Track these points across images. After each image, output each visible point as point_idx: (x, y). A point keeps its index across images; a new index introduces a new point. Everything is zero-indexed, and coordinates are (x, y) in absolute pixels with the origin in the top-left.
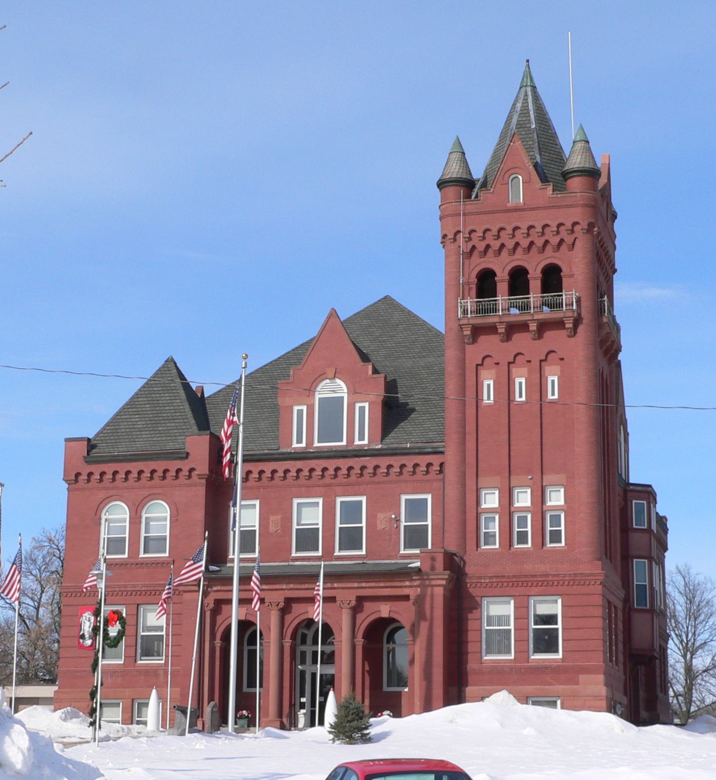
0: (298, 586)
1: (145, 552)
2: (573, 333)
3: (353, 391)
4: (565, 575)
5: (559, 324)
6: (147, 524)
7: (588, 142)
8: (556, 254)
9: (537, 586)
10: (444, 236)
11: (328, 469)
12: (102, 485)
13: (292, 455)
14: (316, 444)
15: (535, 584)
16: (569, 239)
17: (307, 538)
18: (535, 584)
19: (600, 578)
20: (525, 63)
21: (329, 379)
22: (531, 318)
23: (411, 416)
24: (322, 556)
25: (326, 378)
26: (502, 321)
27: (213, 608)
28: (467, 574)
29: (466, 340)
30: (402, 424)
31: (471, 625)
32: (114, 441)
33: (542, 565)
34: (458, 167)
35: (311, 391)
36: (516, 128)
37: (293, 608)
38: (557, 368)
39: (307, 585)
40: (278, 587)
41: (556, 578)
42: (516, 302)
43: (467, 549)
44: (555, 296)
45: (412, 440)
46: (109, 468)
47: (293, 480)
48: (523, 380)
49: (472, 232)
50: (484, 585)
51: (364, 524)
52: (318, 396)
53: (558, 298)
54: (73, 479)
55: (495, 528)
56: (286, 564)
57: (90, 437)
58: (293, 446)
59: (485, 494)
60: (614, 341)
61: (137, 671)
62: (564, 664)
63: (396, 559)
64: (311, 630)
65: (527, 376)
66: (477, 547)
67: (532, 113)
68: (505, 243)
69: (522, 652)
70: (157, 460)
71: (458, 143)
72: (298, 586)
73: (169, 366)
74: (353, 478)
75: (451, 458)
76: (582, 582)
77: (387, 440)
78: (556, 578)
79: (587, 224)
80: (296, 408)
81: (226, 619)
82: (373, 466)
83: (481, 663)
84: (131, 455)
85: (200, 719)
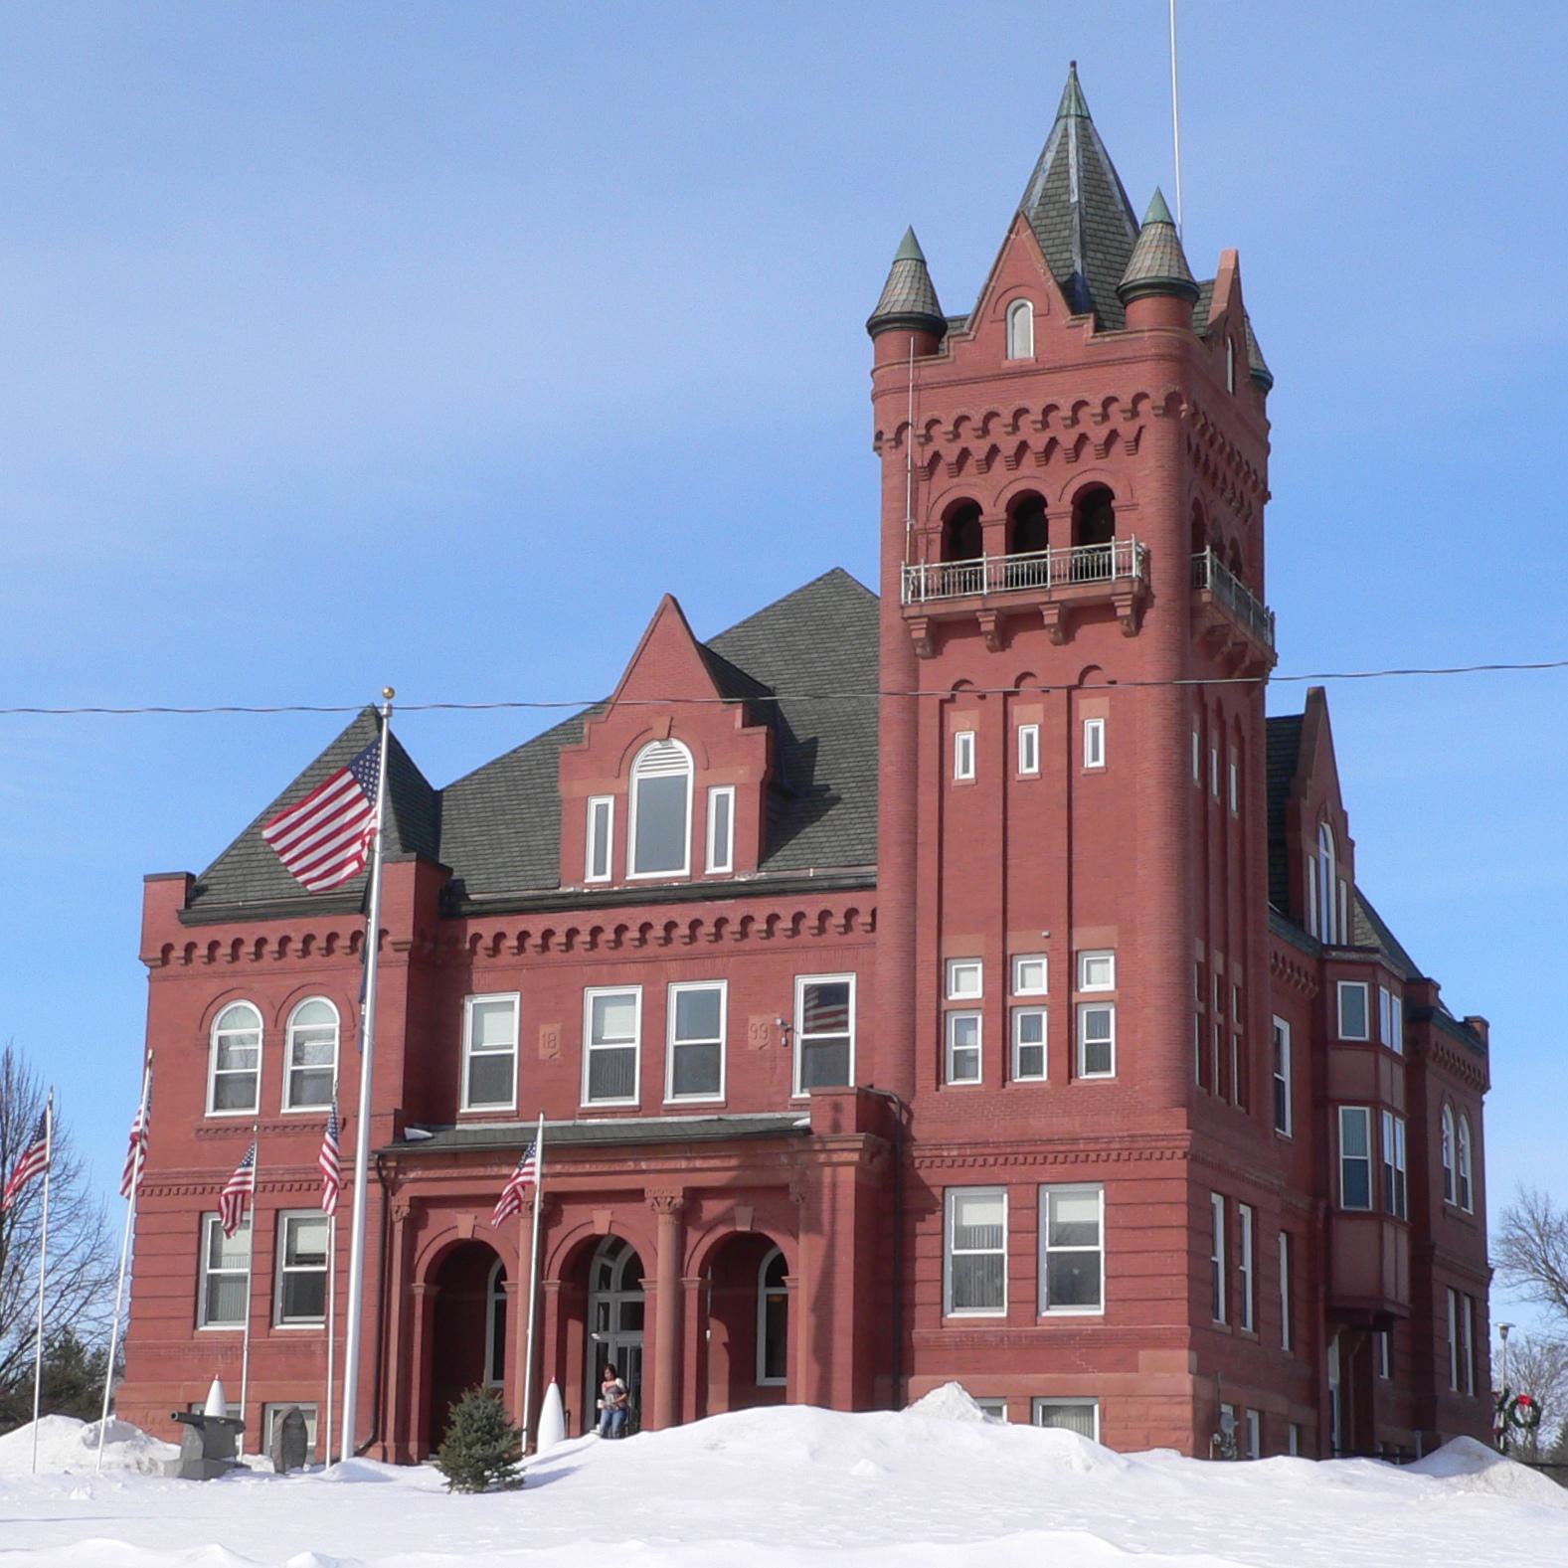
0: (572, 1169)
1: (293, 1102)
2: (1133, 628)
3: (703, 765)
4: (1111, 1139)
5: (1103, 610)
6: (299, 1047)
7: (1171, 225)
8: (1101, 463)
9: (1054, 1163)
10: (879, 436)
11: (650, 927)
12: (214, 967)
13: (581, 900)
14: (632, 875)
15: (1051, 1158)
16: (1127, 430)
17: (612, 1069)
18: (1051, 1158)
19: (1183, 1144)
20: (1069, 69)
21: (659, 740)
22: (1046, 599)
23: (830, 812)
24: (640, 1106)
25: (653, 739)
26: (989, 606)
27: (682, 1206)
28: (914, 1139)
29: (919, 651)
30: (808, 830)
31: (923, 1246)
32: (240, 879)
33: (1067, 1119)
34: (906, 291)
35: (622, 770)
36: (1039, 205)
37: (565, 1213)
38: (1102, 703)
39: (588, 1166)
40: (616, 1167)
41: (1092, 1146)
42: (1017, 566)
43: (918, 1087)
44: (1095, 550)
45: (820, 861)
46: (226, 934)
47: (586, 950)
48: (1035, 730)
49: (932, 423)
50: (948, 1162)
51: (722, 1039)
52: (636, 776)
53: (1101, 554)
54: (160, 957)
55: (975, 1042)
56: (569, 1123)
57: (197, 874)
58: (586, 881)
59: (1023, 966)
60: (1245, 644)
61: (1040, 1337)
62: (1109, 1327)
63: (785, 1109)
64: (619, 1259)
65: (1042, 721)
66: (938, 1082)
67: (1073, 172)
68: (970, 449)
69: (1023, 1306)
70: (316, 915)
71: (912, 239)
72: (572, 1169)
73: (365, 724)
74: (702, 943)
75: (887, 898)
76: (1147, 1154)
77: (771, 864)
78: (1092, 1146)
79: (1163, 397)
80: (594, 802)
81: (435, 1238)
82: (739, 918)
83: (942, 1327)
84: (265, 906)
85: (380, 1443)
